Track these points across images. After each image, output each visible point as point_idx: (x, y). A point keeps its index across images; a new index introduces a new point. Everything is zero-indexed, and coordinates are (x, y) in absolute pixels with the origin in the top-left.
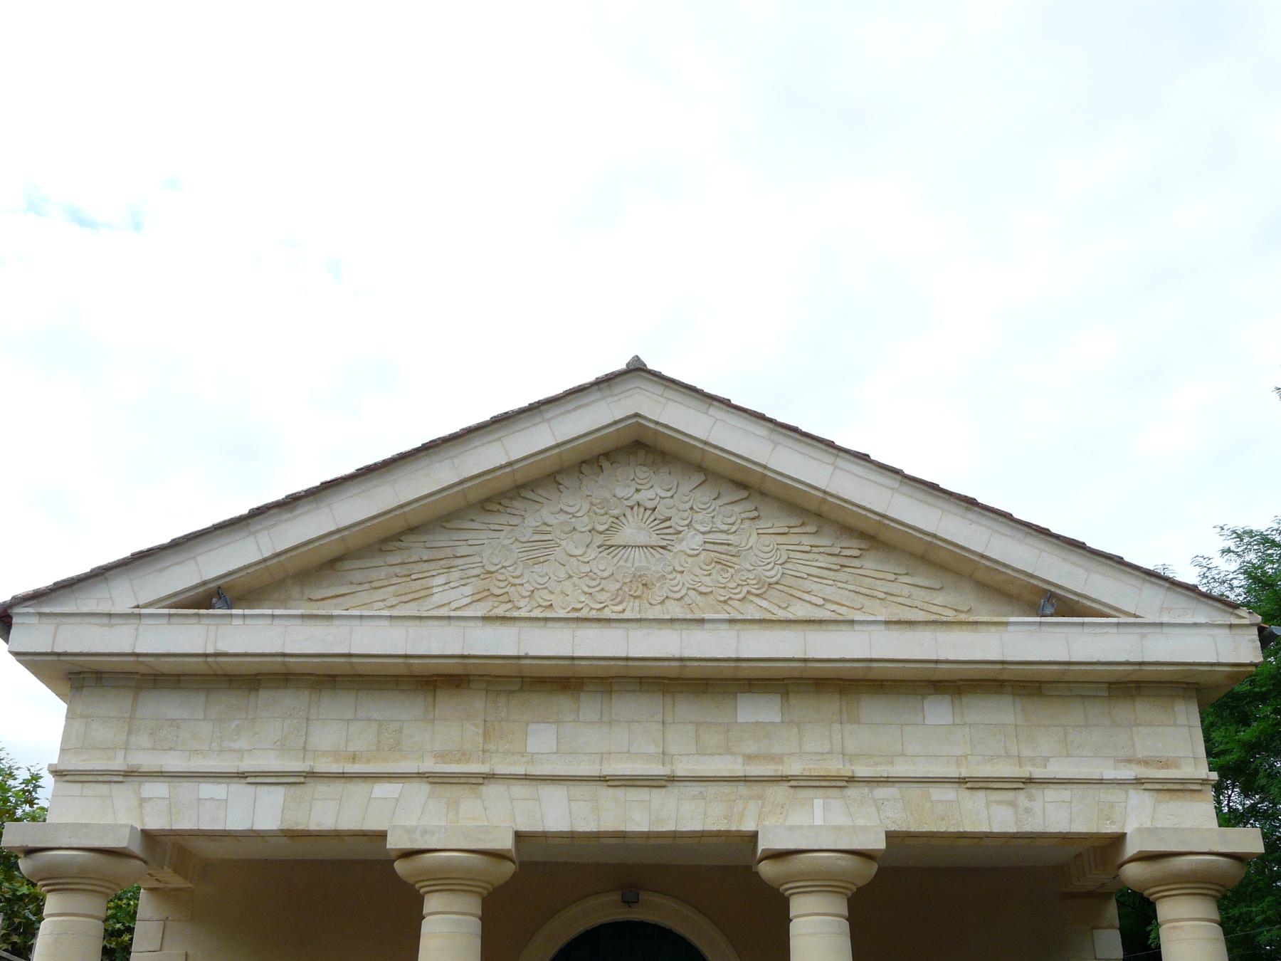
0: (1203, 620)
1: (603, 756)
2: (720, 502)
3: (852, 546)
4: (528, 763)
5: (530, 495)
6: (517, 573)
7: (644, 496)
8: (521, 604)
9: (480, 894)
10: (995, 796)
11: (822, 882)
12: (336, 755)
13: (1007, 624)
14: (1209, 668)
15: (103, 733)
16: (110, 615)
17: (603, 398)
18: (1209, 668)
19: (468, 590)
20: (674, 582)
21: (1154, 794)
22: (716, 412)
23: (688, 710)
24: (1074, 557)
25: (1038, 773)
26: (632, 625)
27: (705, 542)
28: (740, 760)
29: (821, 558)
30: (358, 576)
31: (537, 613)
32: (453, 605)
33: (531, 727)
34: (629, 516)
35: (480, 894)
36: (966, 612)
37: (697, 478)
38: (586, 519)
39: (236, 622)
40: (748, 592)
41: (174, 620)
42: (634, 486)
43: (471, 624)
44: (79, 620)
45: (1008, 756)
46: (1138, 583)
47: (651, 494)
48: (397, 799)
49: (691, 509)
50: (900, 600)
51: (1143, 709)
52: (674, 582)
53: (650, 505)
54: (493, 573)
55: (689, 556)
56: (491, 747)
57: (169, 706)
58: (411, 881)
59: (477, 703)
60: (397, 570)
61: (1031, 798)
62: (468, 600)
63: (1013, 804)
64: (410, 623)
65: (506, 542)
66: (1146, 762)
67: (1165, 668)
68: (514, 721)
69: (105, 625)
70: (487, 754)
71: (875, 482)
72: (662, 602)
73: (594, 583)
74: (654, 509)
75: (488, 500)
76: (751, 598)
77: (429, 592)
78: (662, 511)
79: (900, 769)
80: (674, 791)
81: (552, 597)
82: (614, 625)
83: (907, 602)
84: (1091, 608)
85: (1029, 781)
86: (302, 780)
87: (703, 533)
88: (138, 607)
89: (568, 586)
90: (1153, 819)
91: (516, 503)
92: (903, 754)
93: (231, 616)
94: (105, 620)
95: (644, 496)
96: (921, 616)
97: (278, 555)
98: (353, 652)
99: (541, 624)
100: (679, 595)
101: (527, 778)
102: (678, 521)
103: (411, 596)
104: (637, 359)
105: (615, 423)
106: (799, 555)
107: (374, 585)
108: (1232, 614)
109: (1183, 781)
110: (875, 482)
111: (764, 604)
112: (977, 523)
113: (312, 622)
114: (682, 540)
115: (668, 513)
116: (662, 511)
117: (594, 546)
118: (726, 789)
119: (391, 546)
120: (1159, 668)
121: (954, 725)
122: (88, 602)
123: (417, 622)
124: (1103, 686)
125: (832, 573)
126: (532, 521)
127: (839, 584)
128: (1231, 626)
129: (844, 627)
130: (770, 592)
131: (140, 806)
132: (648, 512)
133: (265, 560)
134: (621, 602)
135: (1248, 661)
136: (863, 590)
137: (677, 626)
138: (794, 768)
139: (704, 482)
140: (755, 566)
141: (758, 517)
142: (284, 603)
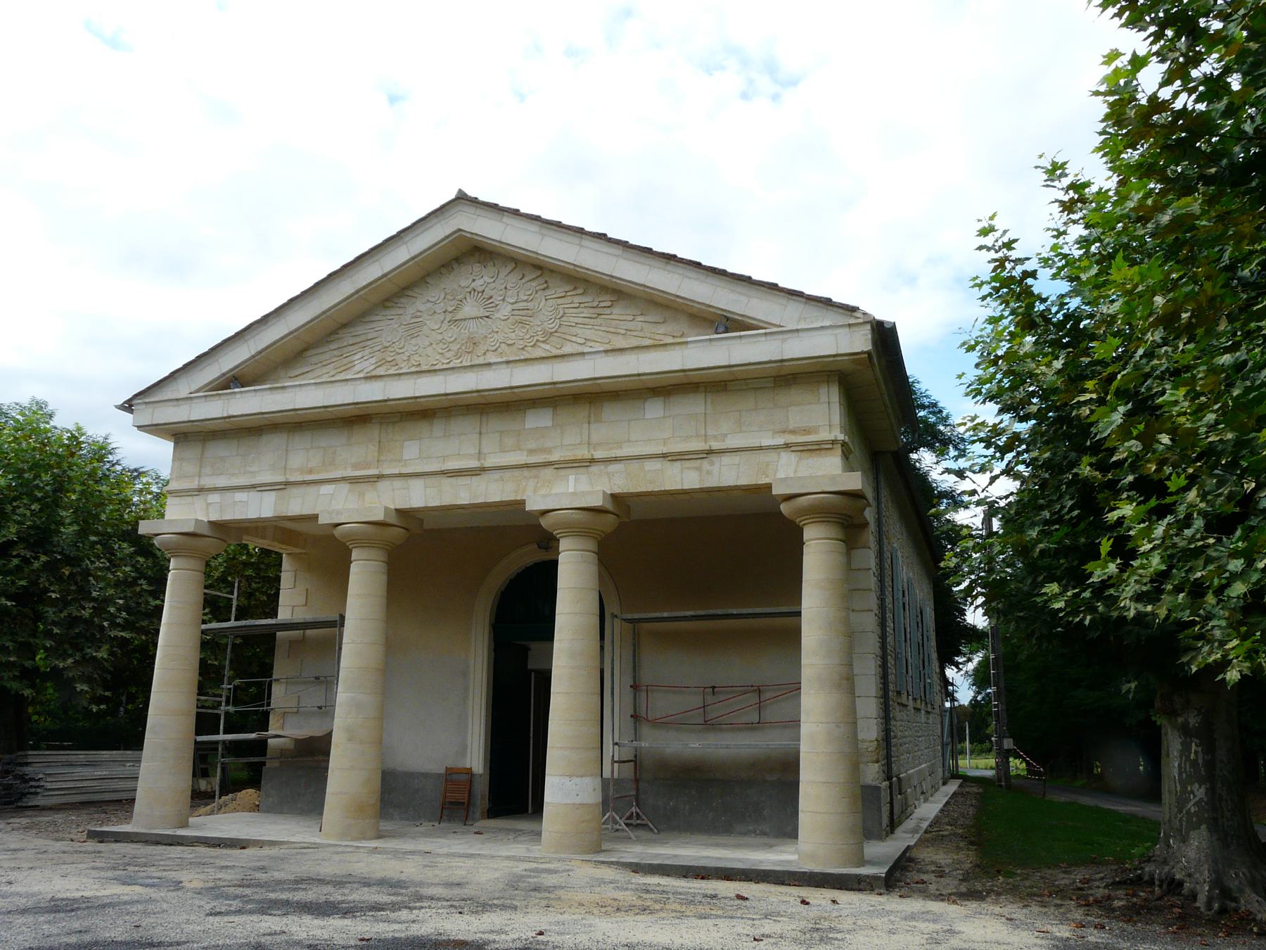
0: (827, 323)
1: (445, 458)
2: (524, 281)
3: (606, 300)
4: (402, 466)
5: (410, 293)
6: (401, 346)
7: (478, 284)
8: (403, 366)
9: (386, 549)
10: (687, 464)
11: (364, 541)
12: (302, 470)
13: (687, 343)
14: (831, 359)
15: (189, 468)
16: (177, 400)
17: (439, 222)
18: (831, 359)
19: (373, 360)
20: (492, 340)
21: (799, 453)
22: (507, 219)
23: (495, 424)
24: (741, 288)
25: (716, 445)
26: (449, 372)
27: (513, 310)
28: (525, 453)
29: (585, 310)
30: (314, 360)
31: (413, 369)
32: (366, 371)
33: (406, 443)
34: (468, 300)
35: (386, 549)
36: (680, 337)
37: (511, 266)
38: (442, 304)
39: (238, 396)
40: (537, 340)
41: (208, 399)
42: (472, 277)
43: (358, 382)
44: (162, 404)
45: (697, 436)
46: (784, 301)
47: (480, 282)
48: (332, 495)
49: (506, 288)
50: (635, 333)
51: (795, 394)
52: (492, 340)
53: (480, 289)
54: (387, 347)
55: (503, 320)
56: (382, 458)
57: (218, 450)
58: (550, 531)
59: (374, 431)
60: (335, 352)
61: (712, 464)
62: (373, 367)
63: (699, 469)
64: (325, 386)
65: (396, 326)
66: (793, 432)
67: (804, 362)
68: (396, 441)
69: (175, 406)
70: (381, 463)
71: (607, 253)
72: (485, 354)
73: (445, 346)
74: (484, 291)
75: (387, 300)
76: (539, 344)
77: (352, 364)
78: (488, 293)
79: (627, 451)
80: (485, 476)
81: (420, 358)
82: (438, 373)
83: (640, 334)
84: (752, 324)
85: (710, 452)
86: (283, 487)
87: (512, 304)
88: (191, 393)
89: (429, 351)
90: (796, 471)
91: (403, 300)
92: (629, 441)
93: (235, 393)
94: (175, 403)
95: (478, 284)
96: (648, 342)
97: (260, 352)
98: (297, 407)
99: (397, 378)
100: (494, 348)
101: (401, 475)
102: (497, 299)
103: (343, 368)
104: (460, 191)
105: (447, 237)
106: (571, 310)
107: (324, 363)
108: (851, 316)
109: (819, 443)
110: (607, 253)
111: (547, 347)
112: (674, 272)
113: (275, 392)
114: (499, 310)
115: (492, 293)
116: (488, 293)
117: (446, 322)
118: (517, 473)
119: (332, 338)
120: (795, 363)
121: (664, 417)
122: (168, 393)
123: (330, 385)
124: (769, 379)
125: (593, 320)
126: (410, 310)
127: (596, 327)
128: (850, 325)
129: (578, 358)
130: (552, 338)
131: (207, 508)
132: (480, 294)
133: (253, 357)
134: (460, 357)
135: (859, 350)
136: (611, 330)
137: (475, 369)
138: (555, 457)
139: (515, 268)
140: (542, 323)
141: (547, 288)
142: (276, 381)
